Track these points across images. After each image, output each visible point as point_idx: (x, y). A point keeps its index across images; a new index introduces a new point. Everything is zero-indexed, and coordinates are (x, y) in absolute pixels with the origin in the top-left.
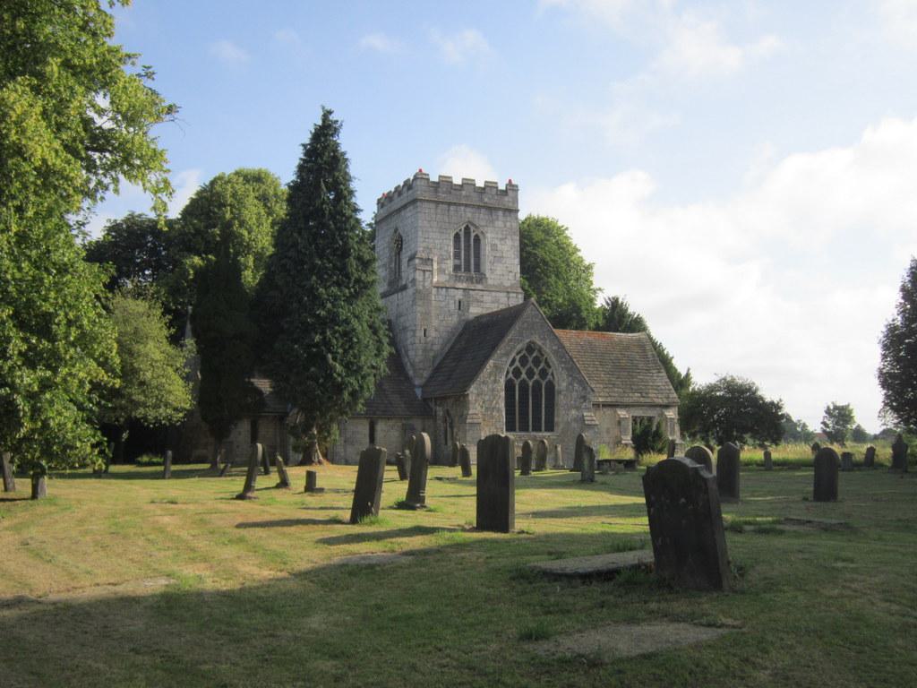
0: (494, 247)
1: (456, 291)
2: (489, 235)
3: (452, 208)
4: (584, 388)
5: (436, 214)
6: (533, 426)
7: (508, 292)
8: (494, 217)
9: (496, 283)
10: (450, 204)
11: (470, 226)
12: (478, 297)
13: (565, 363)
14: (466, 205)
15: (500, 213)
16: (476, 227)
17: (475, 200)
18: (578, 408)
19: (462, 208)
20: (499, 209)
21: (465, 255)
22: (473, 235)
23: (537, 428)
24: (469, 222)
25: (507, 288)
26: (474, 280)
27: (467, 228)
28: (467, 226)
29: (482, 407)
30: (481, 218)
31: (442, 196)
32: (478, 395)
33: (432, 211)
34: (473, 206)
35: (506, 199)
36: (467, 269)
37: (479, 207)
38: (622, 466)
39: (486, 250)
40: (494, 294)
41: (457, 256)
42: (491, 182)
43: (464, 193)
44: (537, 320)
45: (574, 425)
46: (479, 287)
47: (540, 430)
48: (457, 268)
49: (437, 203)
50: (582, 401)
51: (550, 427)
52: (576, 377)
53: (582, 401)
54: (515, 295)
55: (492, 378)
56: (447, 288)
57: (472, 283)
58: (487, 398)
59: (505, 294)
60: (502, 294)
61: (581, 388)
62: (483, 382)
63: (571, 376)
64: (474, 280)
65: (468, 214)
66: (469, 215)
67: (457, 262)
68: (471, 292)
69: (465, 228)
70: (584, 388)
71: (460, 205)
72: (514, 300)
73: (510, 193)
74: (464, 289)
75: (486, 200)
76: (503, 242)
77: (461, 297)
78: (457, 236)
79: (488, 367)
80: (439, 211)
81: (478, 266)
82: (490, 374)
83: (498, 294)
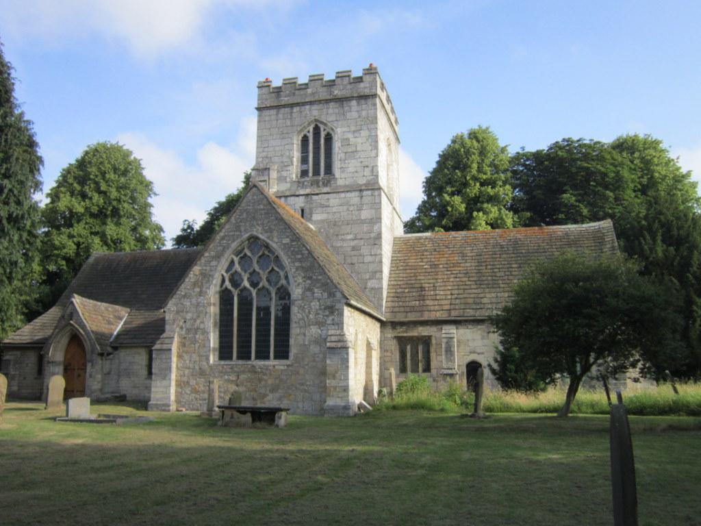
0: (346, 142)
1: (297, 198)
2: (339, 130)
3: (296, 109)
4: (332, 295)
5: (277, 120)
6: (275, 352)
7: (361, 191)
8: (346, 109)
9: (347, 183)
10: (292, 106)
11: (319, 125)
12: (323, 202)
13: (300, 261)
14: (311, 103)
15: (354, 103)
16: (325, 124)
17: (323, 94)
18: (320, 324)
19: (307, 107)
20: (352, 98)
21: (314, 157)
22: (323, 135)
23: (263, 354)
24: (316, 120)
25: (361, 185)
26: (321, 183)
27: (317, 131)
28: (316, 125)
29: (182, 328)
30: (329, 115)
31: (285, 100)
32: (178, 312)
33: (273, 117)
34: (320, 102)
35: (362, 85)
36: (316, 172)
37: (327, 101)
38: (248, 418)
39: (337, 145)
40: (343, 195)
41: (304, 160)
42: (341, 72)
43: (309, 91)
44: (262, 207)
45: (314, 349)
46: (326, 190)
47: (267, 358)
48: (304, 173)
49: (278, 107)
50: (327, 313)
51: (283, 353)
52: (317, 280)
53: (327, 313)
54: (369, 193)
55: (197, 290)
56: (286, 197)
57: (318, 186)
58: (189, 316)
59: (357, 194)
60: (353, 194)
61: (325, 295)
62: (185, 296)
63: (310, 278)
64: (321, 183)
65: (314, 112)
66: (315, 113)
67: (305, 167)
68: (315, 197)
69: (314, 129)
70: (332, 295)
71: (304, 104)
72: (369, 198)
73: (367, 79)
74: (307, 195)
75: (336, 92)
76: (356, 135)
77: (303, 205)
78: (305, 140)
79: (191, 275)
80: (281, 116)
81: (329, 169)
82: (195, 284)
83: (348, 195)
